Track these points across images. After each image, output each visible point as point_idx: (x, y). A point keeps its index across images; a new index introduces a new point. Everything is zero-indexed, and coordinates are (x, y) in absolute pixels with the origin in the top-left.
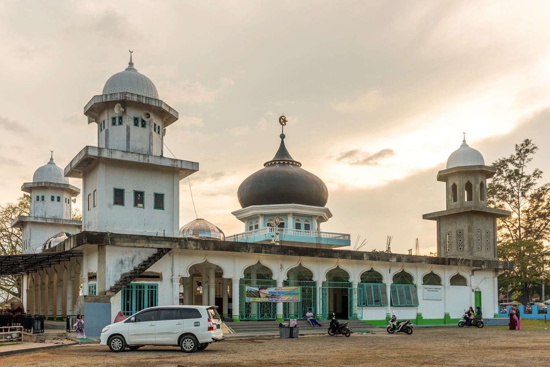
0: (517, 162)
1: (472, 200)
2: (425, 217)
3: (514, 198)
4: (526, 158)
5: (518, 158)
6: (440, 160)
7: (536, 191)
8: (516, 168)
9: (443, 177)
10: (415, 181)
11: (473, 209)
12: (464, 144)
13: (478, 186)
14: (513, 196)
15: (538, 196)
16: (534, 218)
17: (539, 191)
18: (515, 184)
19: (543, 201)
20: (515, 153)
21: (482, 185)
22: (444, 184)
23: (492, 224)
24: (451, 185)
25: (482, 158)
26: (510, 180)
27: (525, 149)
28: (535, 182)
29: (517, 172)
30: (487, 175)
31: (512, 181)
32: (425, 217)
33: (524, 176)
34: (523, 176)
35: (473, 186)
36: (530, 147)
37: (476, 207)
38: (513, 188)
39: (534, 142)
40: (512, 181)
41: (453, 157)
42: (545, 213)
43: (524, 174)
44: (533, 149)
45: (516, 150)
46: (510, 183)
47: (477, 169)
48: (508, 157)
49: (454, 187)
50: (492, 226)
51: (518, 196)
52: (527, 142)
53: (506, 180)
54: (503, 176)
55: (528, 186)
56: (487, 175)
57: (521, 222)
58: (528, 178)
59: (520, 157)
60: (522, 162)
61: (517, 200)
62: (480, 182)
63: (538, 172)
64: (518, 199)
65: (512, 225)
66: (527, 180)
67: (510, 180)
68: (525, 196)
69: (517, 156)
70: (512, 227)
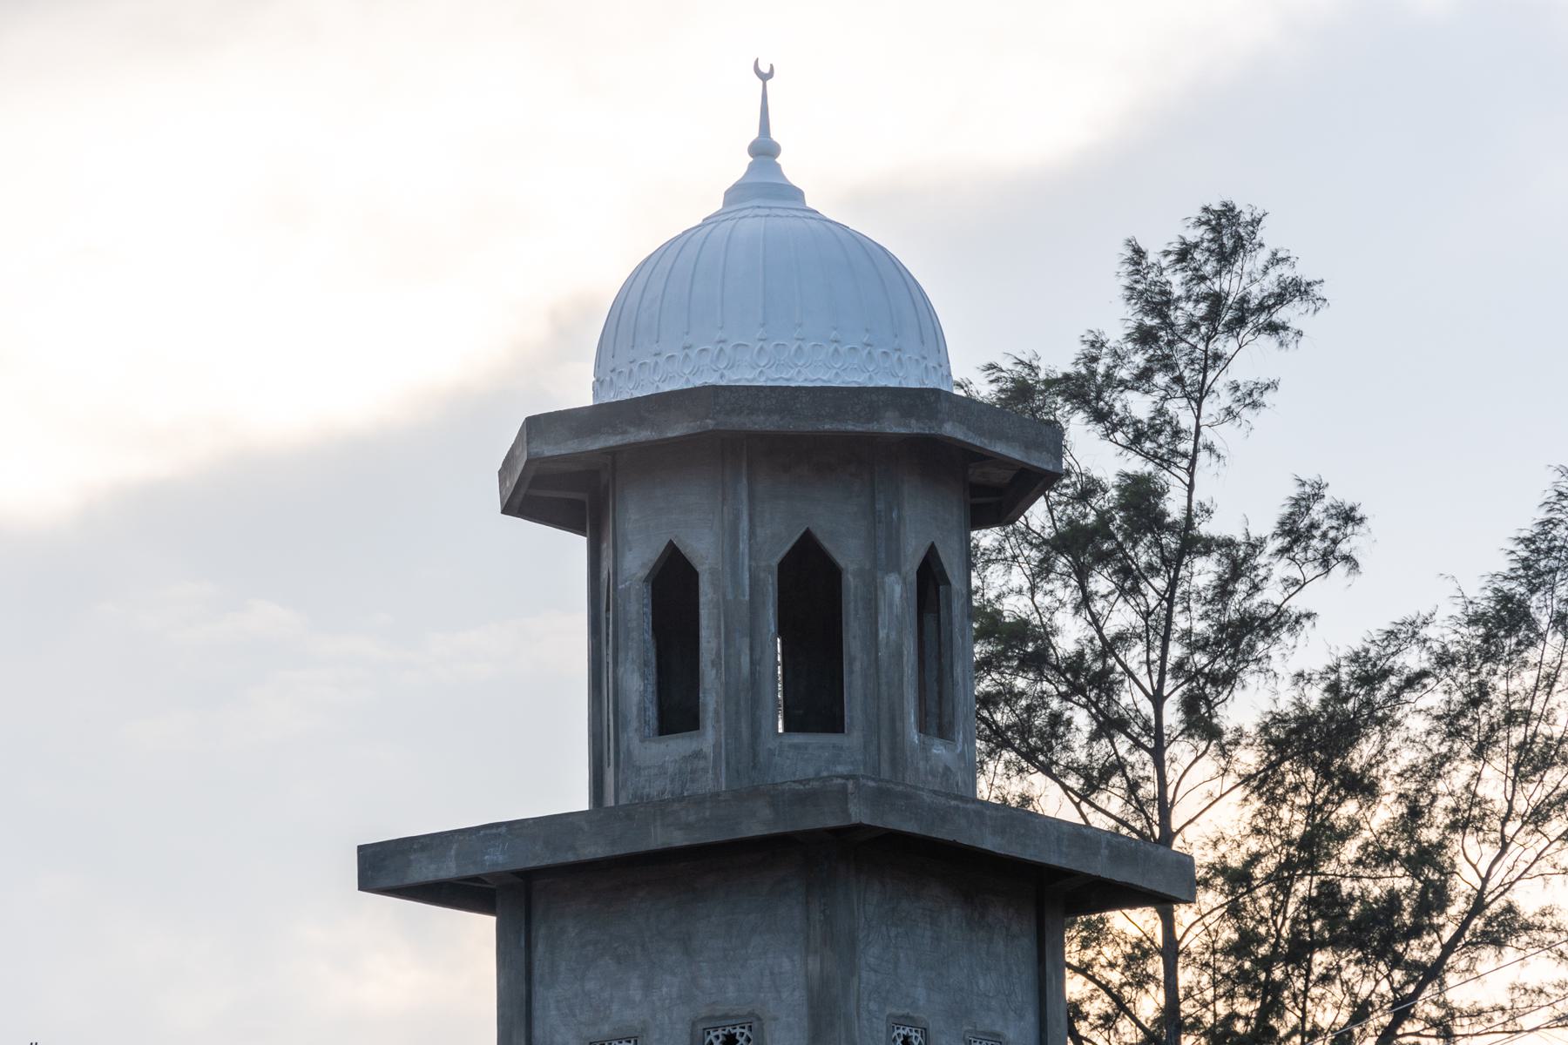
0: (1139, 406)
1: (832, 722)
2: (389, 869)
3: (1123, 744)
4: (1219, 381)
5: (1145, 375)
6: (528, 324)
7: (1314, 696)
8: (1137, 465)
9: (560, 477)
10: (253, 522)
11: (859, 814)
12: (764, 182)
13: (897, 591)
14: (1109, 725)
15: (1320, 741)
16: (1298, 952)
17: (1334, 688)
18: (1121, 617)
19: (1363, 787)
20: (1116, 320)
21: (934, 585)
22: (570, 550)
23: (1025, 975)
24: (637, 561)
25: (926, 331)
26: (1082, 574)
27: (1208, 298)
28: (1297, 605)
29: (1140, 497)
30: (975, 489)
31: (1101, 582)
32: (389, 869)
33: (1207, 546)
34: (1192, 544)
35: (851, 582)
36: (1245, 280)
37: (882, 796)
38: (1110, 647)
39: (1290, 235)
40: (1101, 582)
41: (658, 294)
42: (1393, 898)
43: (1205, 528)
44: (1281, 298)
45: (1132, 293)
46: (1086, 600)
47: (892, 425)
48: (1060, 360)
49: (674, 581)
50: (1024, 996)
51: (1157, 731)
52: (1227, 233)
53: (1043, 570)
54: (1025, 535)
55: (1242, 636)
56: (975, 489)
57: (1186, 977)
58: (1238, 562)
59: (1167, 364)
60: (1180, 410)
61: (1140, 762)
62: (911, 565)
63: (1317, 512)
64: (1158, 755)
65: (1102, 1004)
66: (1223, 591)
67: (1082, 574)
68: (1212, 732)
69: (1139, 359)
70: (1108, 1021)
